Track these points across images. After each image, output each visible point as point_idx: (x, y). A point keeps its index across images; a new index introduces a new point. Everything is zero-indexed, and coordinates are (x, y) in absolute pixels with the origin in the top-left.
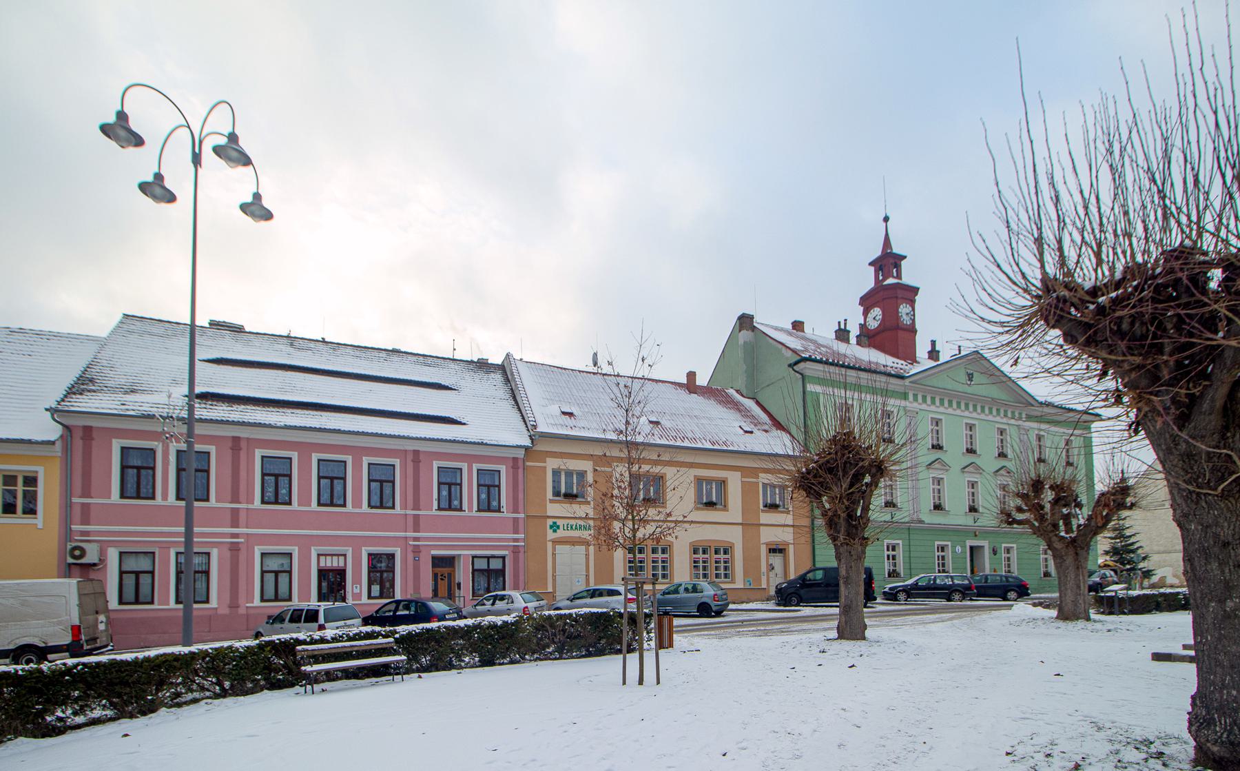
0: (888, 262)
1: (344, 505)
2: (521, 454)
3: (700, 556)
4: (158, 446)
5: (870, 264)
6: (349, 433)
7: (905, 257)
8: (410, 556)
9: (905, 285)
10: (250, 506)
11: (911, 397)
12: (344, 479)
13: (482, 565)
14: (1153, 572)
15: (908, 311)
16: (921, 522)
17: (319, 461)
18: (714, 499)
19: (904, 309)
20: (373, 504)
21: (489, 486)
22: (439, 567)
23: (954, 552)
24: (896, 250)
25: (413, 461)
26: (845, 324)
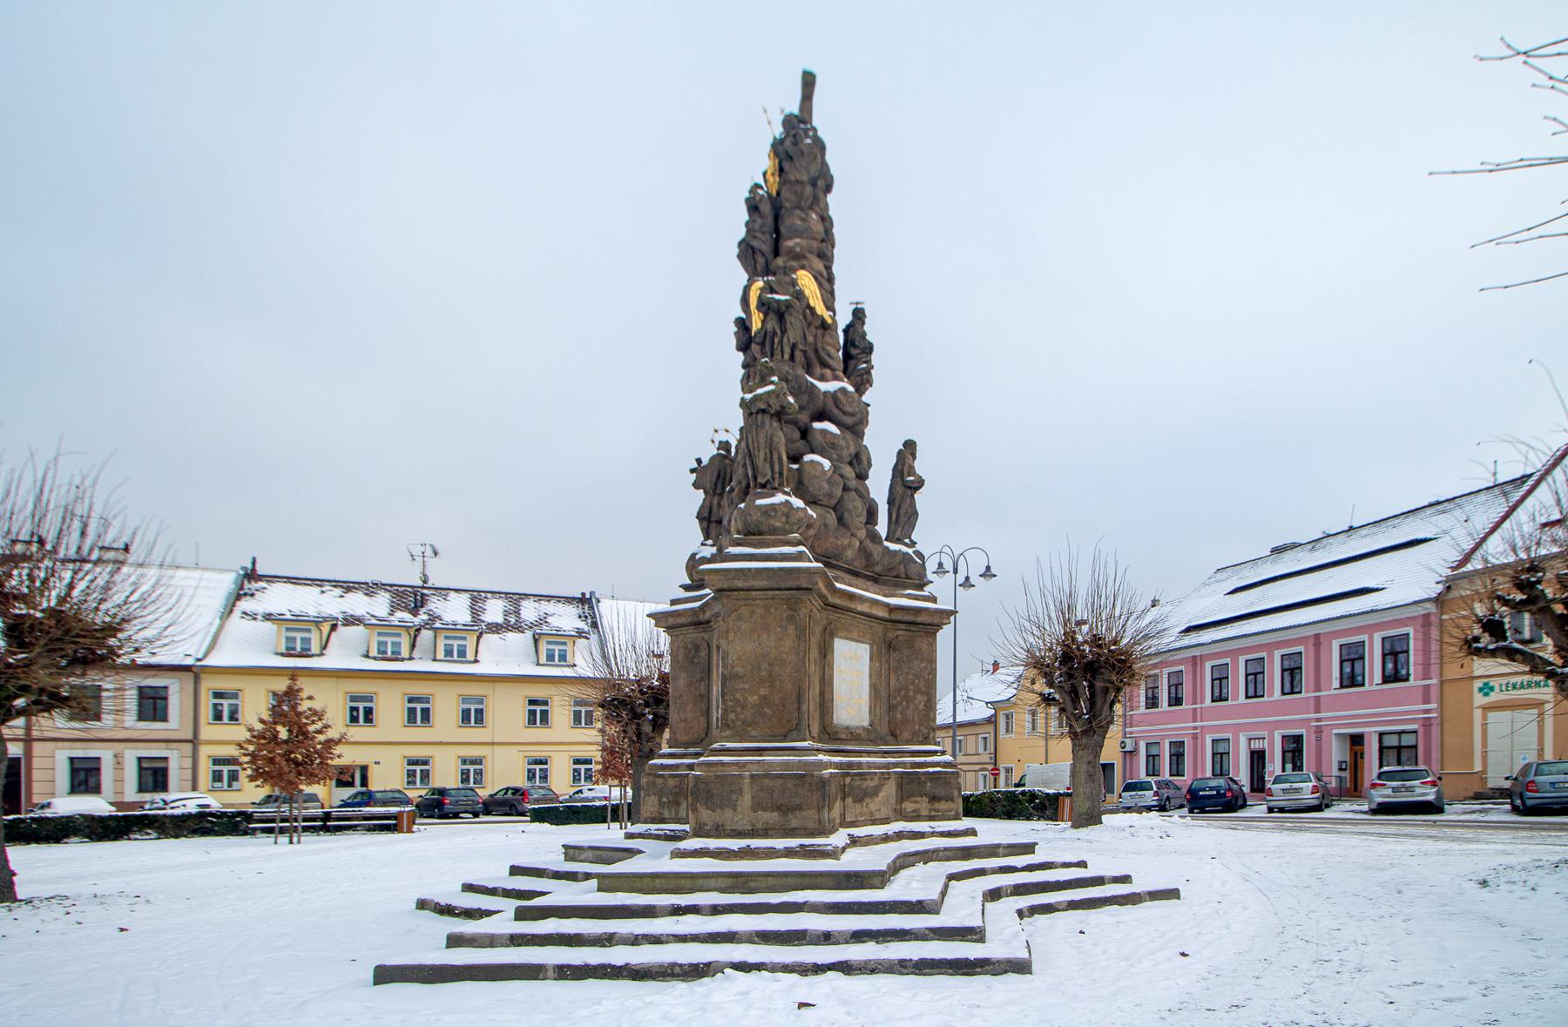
2: (1431, 608)
8: (1313, 736)
10: (1203, 705)
13: (1391, 741)
21: (1292, 673)
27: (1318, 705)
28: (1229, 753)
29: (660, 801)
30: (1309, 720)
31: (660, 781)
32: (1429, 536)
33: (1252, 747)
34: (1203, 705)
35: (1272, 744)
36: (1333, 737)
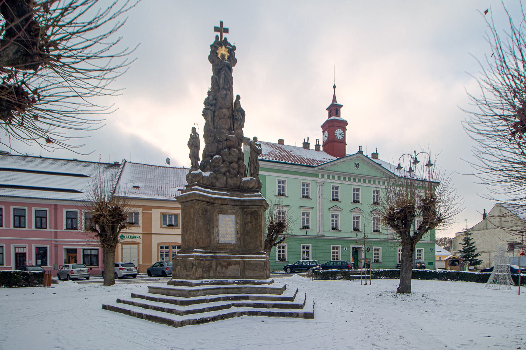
1: (25, 227)
3: (164, 250)
5: (327, 109)
7: (342, 106)
8: (53, 249)
9: (342, 121)
11: (320, 176)
12: (46, 218)
13: (88, 252)
14: (482, 262)
15: (341, 133)
16: (323, 235)
19: (338, 132)
20: (37, 226)
22: (70, 253)
23: (342, 250)
24: (339, 102)
25: (54, 209)
26: (308, 140)
27: (56, 235)
29: (203, 270)
30: (51, 241)
31: (202, 262)
35: (30, 250)
36: (63, 249)
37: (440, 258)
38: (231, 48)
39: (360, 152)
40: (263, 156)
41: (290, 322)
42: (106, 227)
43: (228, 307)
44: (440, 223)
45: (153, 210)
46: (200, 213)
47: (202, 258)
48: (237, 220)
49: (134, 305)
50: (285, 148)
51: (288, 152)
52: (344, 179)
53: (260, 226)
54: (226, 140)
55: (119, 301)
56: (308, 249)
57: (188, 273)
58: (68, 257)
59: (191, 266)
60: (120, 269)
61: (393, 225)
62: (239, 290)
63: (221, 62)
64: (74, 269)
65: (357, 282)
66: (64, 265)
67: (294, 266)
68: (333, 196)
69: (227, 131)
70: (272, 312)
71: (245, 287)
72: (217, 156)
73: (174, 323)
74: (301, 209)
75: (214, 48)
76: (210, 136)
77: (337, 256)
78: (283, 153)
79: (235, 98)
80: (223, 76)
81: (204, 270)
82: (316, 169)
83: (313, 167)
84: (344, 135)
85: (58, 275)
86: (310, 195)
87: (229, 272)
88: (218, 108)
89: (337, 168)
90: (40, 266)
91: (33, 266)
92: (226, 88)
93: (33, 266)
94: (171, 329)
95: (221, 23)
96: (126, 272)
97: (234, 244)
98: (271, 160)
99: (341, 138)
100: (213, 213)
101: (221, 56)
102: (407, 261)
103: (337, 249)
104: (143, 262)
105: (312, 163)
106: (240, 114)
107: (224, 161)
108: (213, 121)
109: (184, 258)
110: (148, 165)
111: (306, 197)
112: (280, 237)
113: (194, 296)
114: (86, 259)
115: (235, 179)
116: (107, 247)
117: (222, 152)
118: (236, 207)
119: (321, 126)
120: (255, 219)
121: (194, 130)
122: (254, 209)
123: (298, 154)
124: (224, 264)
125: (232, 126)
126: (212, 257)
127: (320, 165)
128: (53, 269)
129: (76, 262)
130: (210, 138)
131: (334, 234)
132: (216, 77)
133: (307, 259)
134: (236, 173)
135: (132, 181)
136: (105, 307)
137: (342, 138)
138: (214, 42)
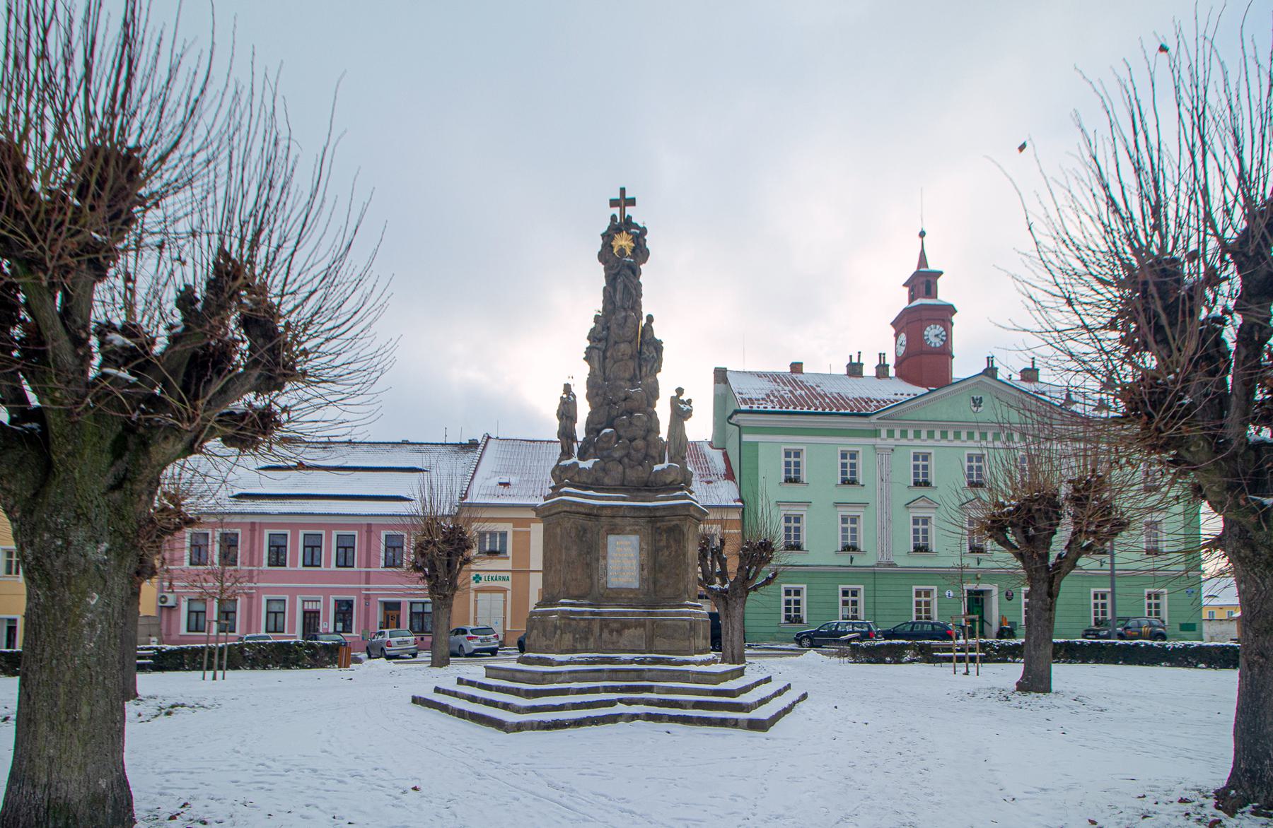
0: (924, 282)
1: (320, 566)
4: (210, 532)
6: (319, 514)
7: (941, 273)
8: (363, 602)
10: (261, 568)
11: (884, 433)
15: (937, 332)
17: (305, 535)
18: (498, 549)
19: (932, 334)
20: (339, 564)
21: (229, 543)
22: (390, 609)
24: (933, 266)
26: (859, 357)
28: (284, 613)
29: (574, 637)
30: (360, 589)
31: (574, 623)
32: (419, 467)
33: (306, 607)
34: (261, 568)
37: (1212, 613)
38: (638, 232)
39: (990, 371)
40: (754, 404)
41: (718, 735)
42: (437, 563)
43: (611, 703)
44: (1122, 530)
45: (532, 525)
46: (573, 535)
47: (573, 615)
48: (642, 544)
49: (457, 697)
50: (804, 380)
51: (812, 387)
52: (944, 435)
53: (684, 555)
54: (626, 399)
55: (437, 690)
56: (799, 595)
57: (548, 642)
58: (387, 617)
59: (553, 629)
60: (469, 638)
61: (1002, 539)
62: (639, 674)
63: (618, 260)
64: (392, 639)
65: (947, 668)
66: (378, 630)
67: (817, 633)
68: (916, 475)
69: (628, 382)
70: (688, 716)
71: (650, 670)
72: (608, 430)
73: (504, 725)
74: (839, 509)
75: (608, 237)
76: (597, 395)
77: (927, 611)
78: (799, 392)
79: (644, 321)
80: (620, 287)
81: (577, 636)
82: (874, 419)
83: (866, 416)
84: (947, 336)
85: (368, 650)
86: (861, 478)
87: (623, 642)
88: (611, 342)
89: (926, 414)
90: (339, 633)
91: (328, 633)
92: (626, 306)
93: (328, 633)
94: (500, 735)
95: (623, 191)
96: (479, 645)
97: (636, 589)
98: (769, 409)
99: (938, 345)
100: (598, 534)
101: (617, 252)
102: (1039, 618)
103: (927, 593)
104: (511, 627)
105: (864, 407)
106: (652, 348)
107: (619, 438)
108: (603, 368)
109: (544, 615)
110: (527, 441)
111: (849, 481)
112: (767, 571)
113: (552, 682)
114: (415, 621)
115: (641, 468)
116: (439, 599)
117: (616, 422)
118: (641, 521)
119: (891, 324)
120: (675, 540)
121: (567, 388)
122: (673, 523)
123: (834, 390)
124: (615, 626)
125: (638, 372)
126: (592, 613)
127: (884, 410)
128: (361, 639)
129: (398, 626)
130: (597, 399)
131: (921, 561)
132: (608, 288)
133: (854, 618)
134: (641, 458)
135: (497, 473)
136: (415, 700)
137: (942, 343)
138: (609, 228)
